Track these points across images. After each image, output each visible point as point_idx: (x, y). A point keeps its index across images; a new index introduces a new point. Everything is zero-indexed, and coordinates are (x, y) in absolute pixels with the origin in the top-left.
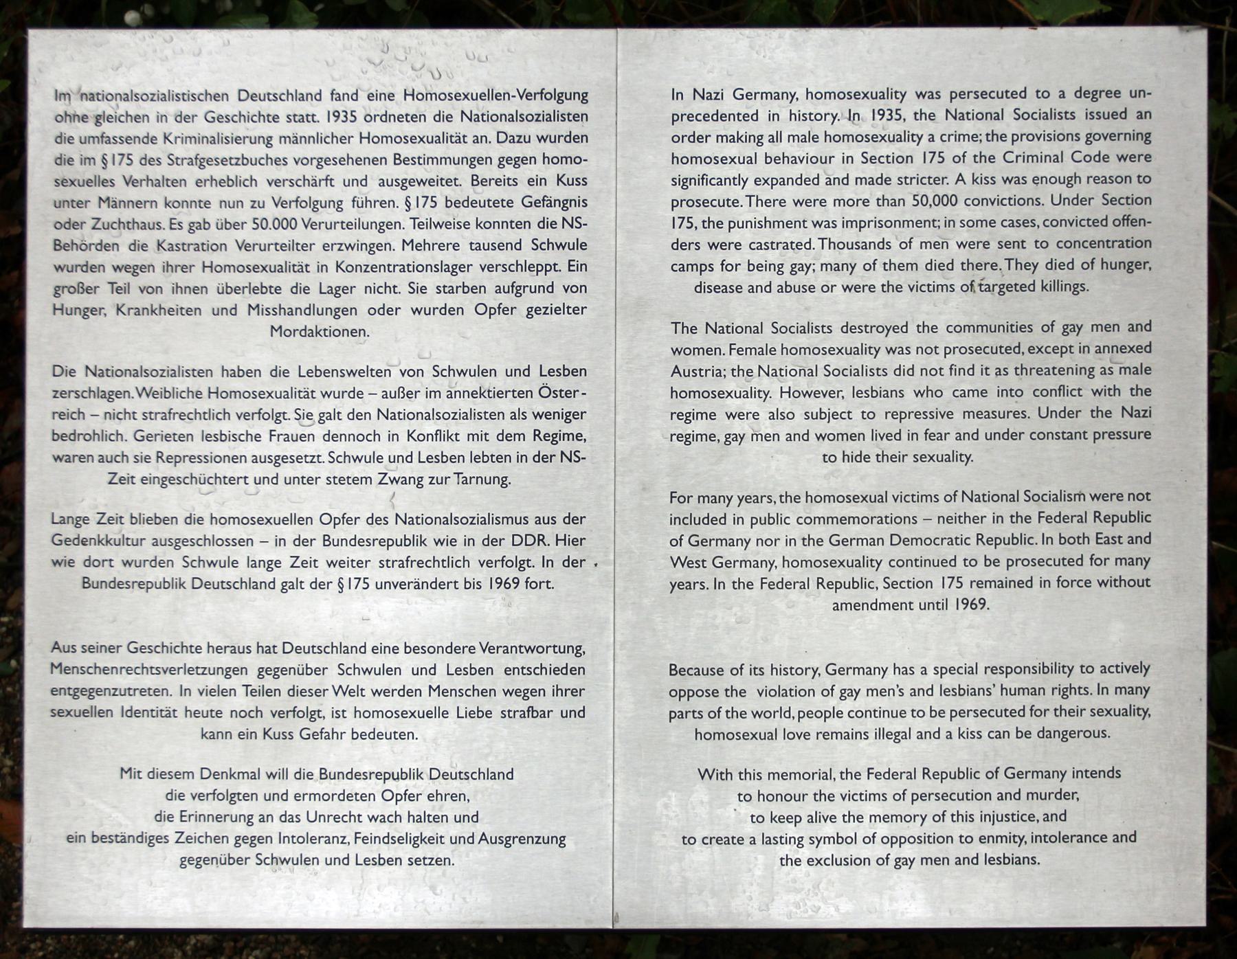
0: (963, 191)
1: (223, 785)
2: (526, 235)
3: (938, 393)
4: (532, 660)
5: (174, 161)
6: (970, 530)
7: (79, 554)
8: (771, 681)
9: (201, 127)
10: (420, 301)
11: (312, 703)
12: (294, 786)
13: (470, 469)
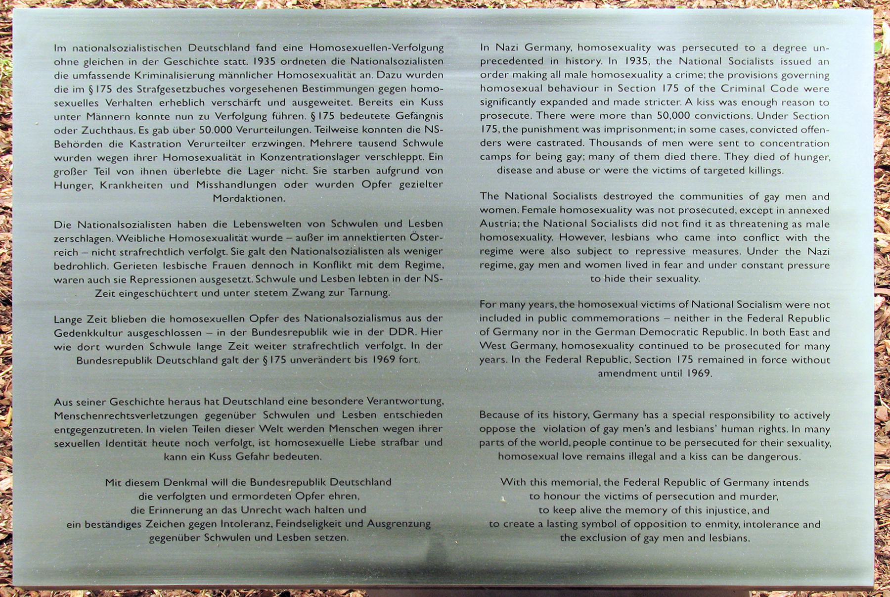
0: (694, 109)
1: (180, 490)
2: (399, 137)
3: (675, 238)
4: (405, 408)
5: (141, 89)
6: (698, 326)
7: (74, 342)
8: (555, 422)
9: (160, 68)
10: (321, 178)
11: (245, 437)
12: (231, 489)
13: (360, 286)
